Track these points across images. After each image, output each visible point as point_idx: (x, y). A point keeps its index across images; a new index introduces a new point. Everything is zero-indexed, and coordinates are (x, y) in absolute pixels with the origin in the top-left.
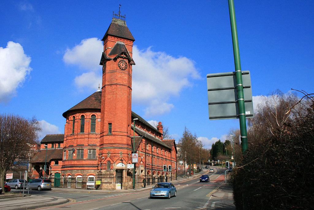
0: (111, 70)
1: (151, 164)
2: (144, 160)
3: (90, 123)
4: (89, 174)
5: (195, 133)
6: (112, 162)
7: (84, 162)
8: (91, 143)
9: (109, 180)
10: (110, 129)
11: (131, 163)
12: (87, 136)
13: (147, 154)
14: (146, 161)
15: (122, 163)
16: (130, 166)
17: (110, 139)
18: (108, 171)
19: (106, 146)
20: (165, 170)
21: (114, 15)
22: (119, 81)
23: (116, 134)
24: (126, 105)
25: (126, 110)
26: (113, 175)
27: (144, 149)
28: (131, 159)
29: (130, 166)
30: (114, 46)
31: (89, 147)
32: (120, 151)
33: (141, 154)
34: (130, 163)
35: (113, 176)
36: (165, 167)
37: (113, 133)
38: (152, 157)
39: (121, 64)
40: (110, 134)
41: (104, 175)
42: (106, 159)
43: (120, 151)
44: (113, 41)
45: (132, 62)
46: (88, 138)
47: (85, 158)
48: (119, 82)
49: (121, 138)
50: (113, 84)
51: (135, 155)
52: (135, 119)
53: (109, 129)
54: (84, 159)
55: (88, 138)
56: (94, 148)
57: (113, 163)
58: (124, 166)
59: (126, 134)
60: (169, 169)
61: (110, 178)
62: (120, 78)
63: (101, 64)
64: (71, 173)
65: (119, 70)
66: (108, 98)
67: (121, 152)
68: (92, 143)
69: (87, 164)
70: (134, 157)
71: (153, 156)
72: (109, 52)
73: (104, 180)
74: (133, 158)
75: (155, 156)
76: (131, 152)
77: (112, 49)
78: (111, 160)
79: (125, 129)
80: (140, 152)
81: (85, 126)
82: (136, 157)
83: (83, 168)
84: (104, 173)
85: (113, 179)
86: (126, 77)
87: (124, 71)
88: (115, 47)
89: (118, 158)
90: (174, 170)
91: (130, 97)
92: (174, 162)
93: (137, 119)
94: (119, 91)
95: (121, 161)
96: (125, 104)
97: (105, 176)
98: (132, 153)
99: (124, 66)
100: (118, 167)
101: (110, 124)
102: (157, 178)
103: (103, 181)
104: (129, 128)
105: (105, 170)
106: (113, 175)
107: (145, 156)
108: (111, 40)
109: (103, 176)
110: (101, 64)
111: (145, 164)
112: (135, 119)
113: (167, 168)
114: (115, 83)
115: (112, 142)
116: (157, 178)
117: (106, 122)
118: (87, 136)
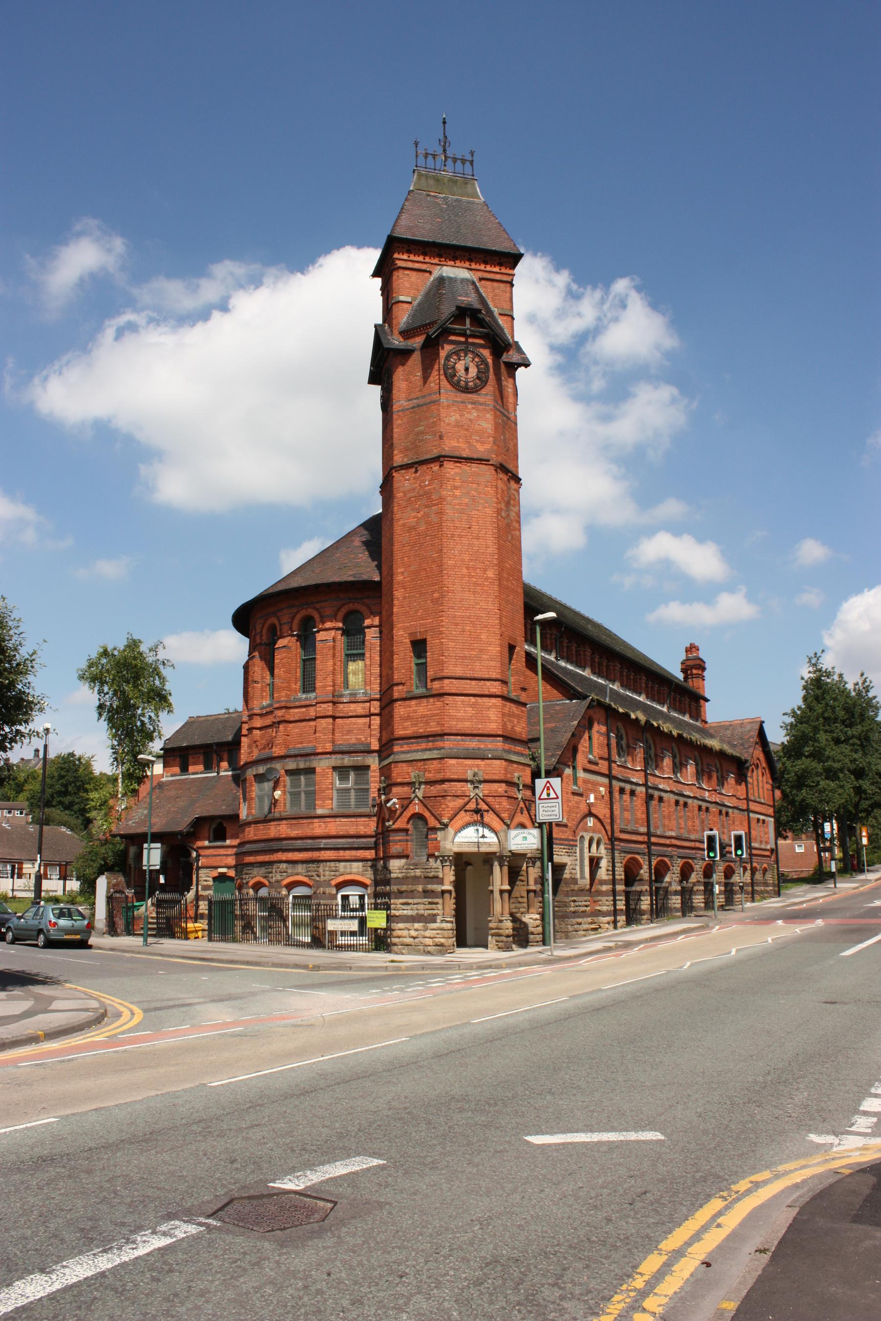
0: (413, 396)
1: (643, 830)
2: (602, 811)
3: (338, 649)
4: (341, 879)
5: (426, 378)
6: (432, 822)
7: (319, 828)
8: (346, 740)
9: (420, 907)
10: (422, 668)
11: (527, 822)
12: (328, 709)
13: (622, 785)
14: (617, 812)
15: (484, 825)
16: (520, 837)
17: (423, 716)
18: (416, 866)
19: (406, 748)
20: (712, 855)
21: (421, 160)
22: (454, 444)
23: (447, 689)
24: (492, 549)
25: (490, 574)
26: (441, 881)
27: (601, 761)
28: (529, 805)
29: (520, 837)
30: (423, 292)
31: (335, 760)
32: (470, 767)
33: (586, 781)
34: (523, 826)
35: (439, 888)
36: (711, 839)
37: (436, 685)
38: (649, 798)
39: (460, 366)
40: (421, 691)
41: (400, 881)
42: (404, 808)
43: (471, 768)
44: (417, 266)
45: (512, 356)
46: (334, 718)
47: (322, 807)
48: (452, 445)
49: (473, 706)
50: (428, 457)
51: (548, 787)
52: (540, 617)
53: (414, 668)
54: (319, 812)
55: (334, 718)
56: (358, 759)
57: (438, 826)
58: (491, 838)
59: (495, 688)
60: (736, 850)
61: (426, 893)
62: (458, 425)
63: (373, 380)
64: (265, 877)
65: (448, 395)
66: (404, 525)
67: (475, 775)
68: (352, 739)
69: (333, 833)
70: (544, 796)
71: (656, 794)
72: (403, 317)
73: (399, 907)
74: (538, 801)
75: (663, 794)
76: (528, 772)
77: (415, 303)
78: (427, 814)
79: (493, 663)
80: (581, 774)
81: (318, 662)
82: (553, 795)
83: (315, 855)
84: (400, 875)
85: (440, 901)
86: (487, 423)
87: (474, 397)
88: (427, 294)
89: (460, 802)
90: (768, 853)
91: (513, 514)
92: (762, 817)
93: (551, 615)
94: (456, 488)
95: (477, 817)
96: (488, 545)
97: (404, 888)
98: (536, 775)
99: (473, 371)
100: (461, 844)
101: (419, 646)
102: (676, 893)
103: (397, 913)
104: (519, 661)
105: (403, 861)
106: (441, 881)
107: (611, 793)
108: (410, 265)
109: (394, 888)
110: (373, 380)
111: (608, 828)
112: (540, 617)
113: (722, 847)
114: (435, 453)
115: (434, 728)
116: (676, 893)
117: (402, 637)
118: (328, 709)
